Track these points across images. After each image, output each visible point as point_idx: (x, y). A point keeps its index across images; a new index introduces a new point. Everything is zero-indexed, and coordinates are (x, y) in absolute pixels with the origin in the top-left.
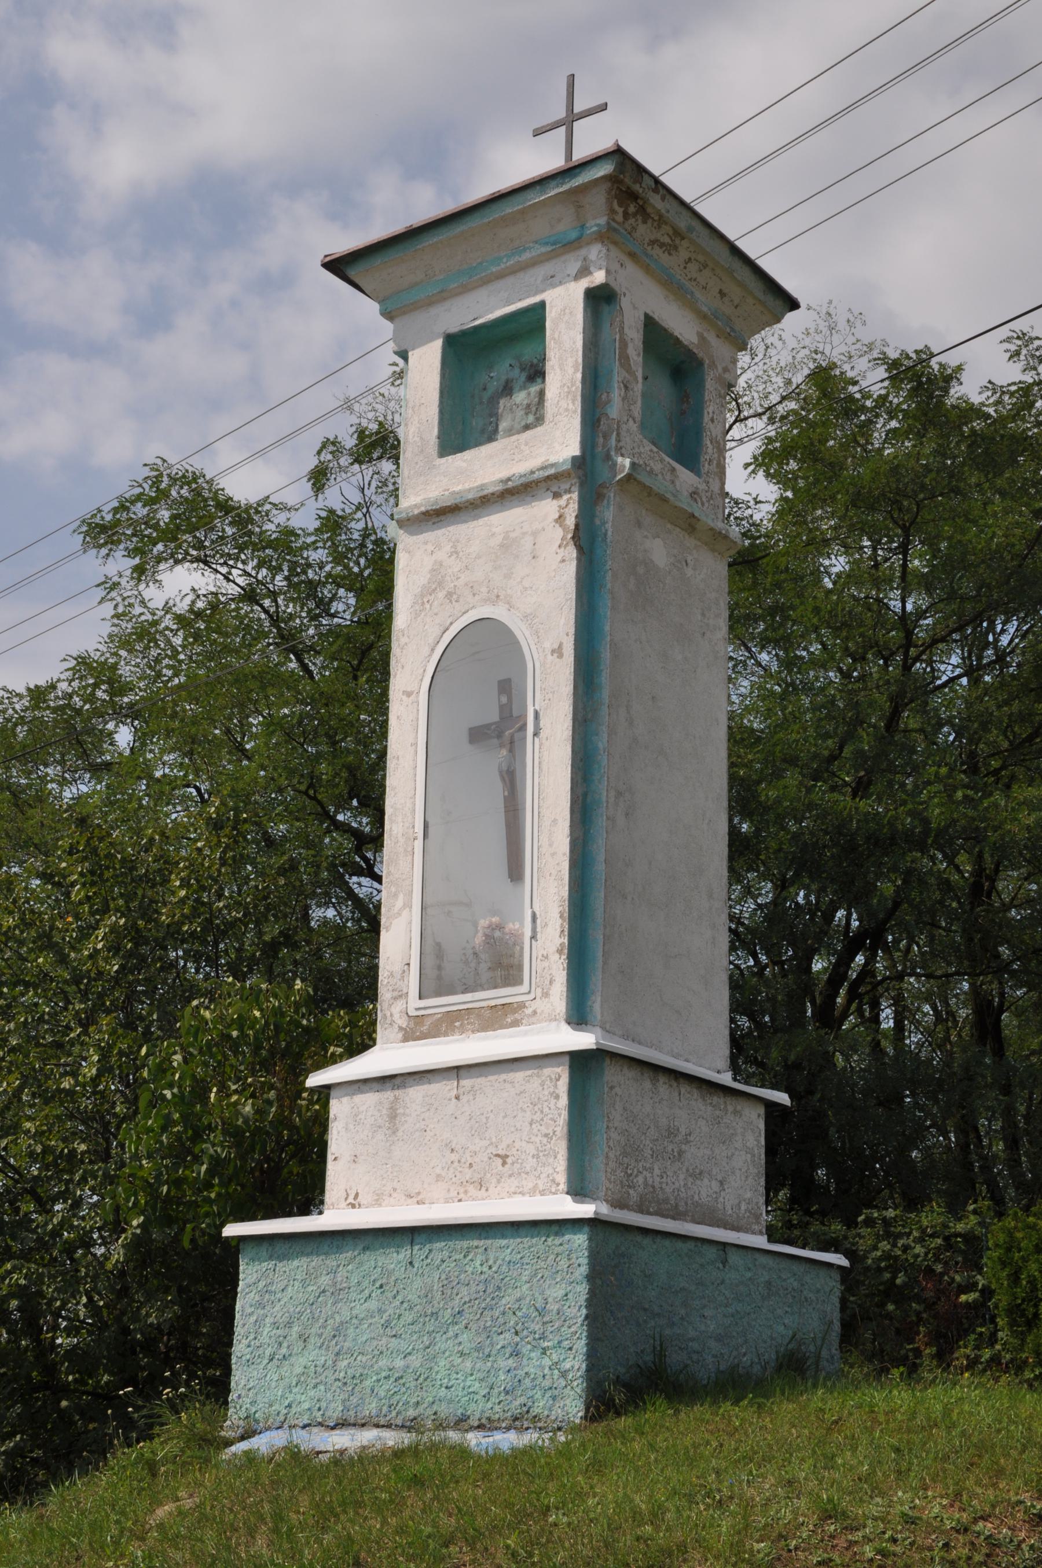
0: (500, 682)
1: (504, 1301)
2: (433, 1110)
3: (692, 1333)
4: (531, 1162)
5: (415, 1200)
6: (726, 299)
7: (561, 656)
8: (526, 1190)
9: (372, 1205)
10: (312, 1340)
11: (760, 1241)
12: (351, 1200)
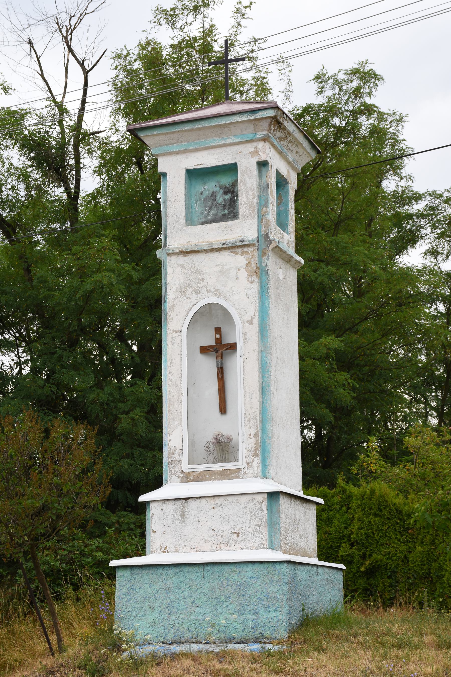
1: (249, 593)
2: (202, 513)
3: (311, 602)
4: (250, 536)
5: (195, 550)
6: (297, 154)
7: (252, 324)
8: (248, 547)
9: (174, 552)
10: (156, 609)
11: (316, 561)
12: (163, 549)
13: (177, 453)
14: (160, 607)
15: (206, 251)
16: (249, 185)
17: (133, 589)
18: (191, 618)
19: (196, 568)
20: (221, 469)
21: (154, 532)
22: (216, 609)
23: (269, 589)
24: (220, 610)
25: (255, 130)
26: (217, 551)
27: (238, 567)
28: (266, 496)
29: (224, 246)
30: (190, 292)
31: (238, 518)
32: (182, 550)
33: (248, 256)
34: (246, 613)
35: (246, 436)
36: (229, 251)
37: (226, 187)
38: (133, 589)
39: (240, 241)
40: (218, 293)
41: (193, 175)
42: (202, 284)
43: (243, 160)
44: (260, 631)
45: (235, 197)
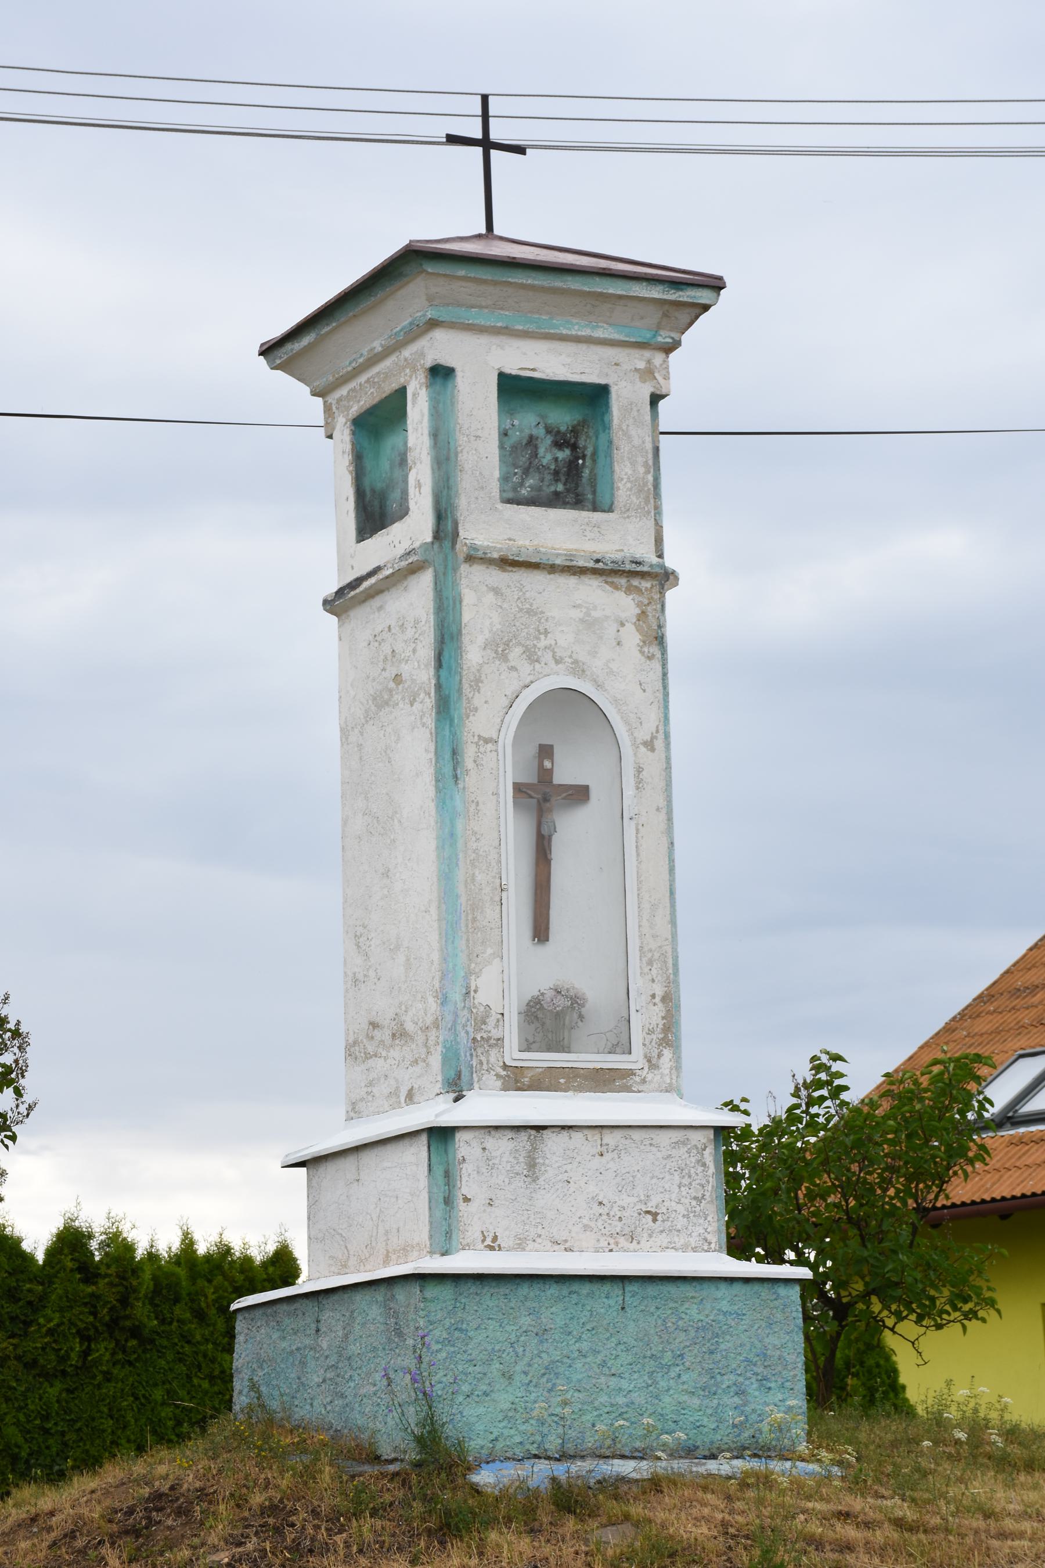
0: (552, 747)
2: (575, 1164)
4: (681, 1222)
7: (653, 750)
8: (678, 1245)
12: (488, 1242)
13: (492, 1021)
14: (526, 1373)
15: (552, 569)
16: (636, 442)
17: (461, 1330)
18: (602, 1400)
19: (607, 1287)
20: (591, 1066)
21: (467, 1200)
22: (655, 1383)
23: (767, 1340)
24: (663, 1384)
25: (659, 323)
26: (611, 1251)
27: (698, 1287)
28: (711, 1134)
29: (597, 566)
30: (515, 653)
31: (654, 1181)
32: (531, 1245)
33: (641, 599)
34: (720, 1391)
35: (645, 998)
36: (601, 579)
37: (558, 432)
38: (461, 1330)
39: (632, 562)
40: (578, 669)
41: (514, 389)
42: (543, 643)
43: (623, 384)
44: (751, 1432)
45: (578, 458)
